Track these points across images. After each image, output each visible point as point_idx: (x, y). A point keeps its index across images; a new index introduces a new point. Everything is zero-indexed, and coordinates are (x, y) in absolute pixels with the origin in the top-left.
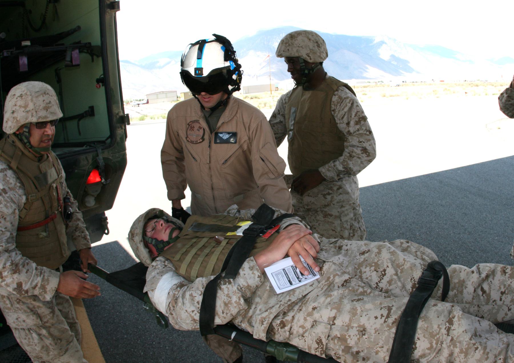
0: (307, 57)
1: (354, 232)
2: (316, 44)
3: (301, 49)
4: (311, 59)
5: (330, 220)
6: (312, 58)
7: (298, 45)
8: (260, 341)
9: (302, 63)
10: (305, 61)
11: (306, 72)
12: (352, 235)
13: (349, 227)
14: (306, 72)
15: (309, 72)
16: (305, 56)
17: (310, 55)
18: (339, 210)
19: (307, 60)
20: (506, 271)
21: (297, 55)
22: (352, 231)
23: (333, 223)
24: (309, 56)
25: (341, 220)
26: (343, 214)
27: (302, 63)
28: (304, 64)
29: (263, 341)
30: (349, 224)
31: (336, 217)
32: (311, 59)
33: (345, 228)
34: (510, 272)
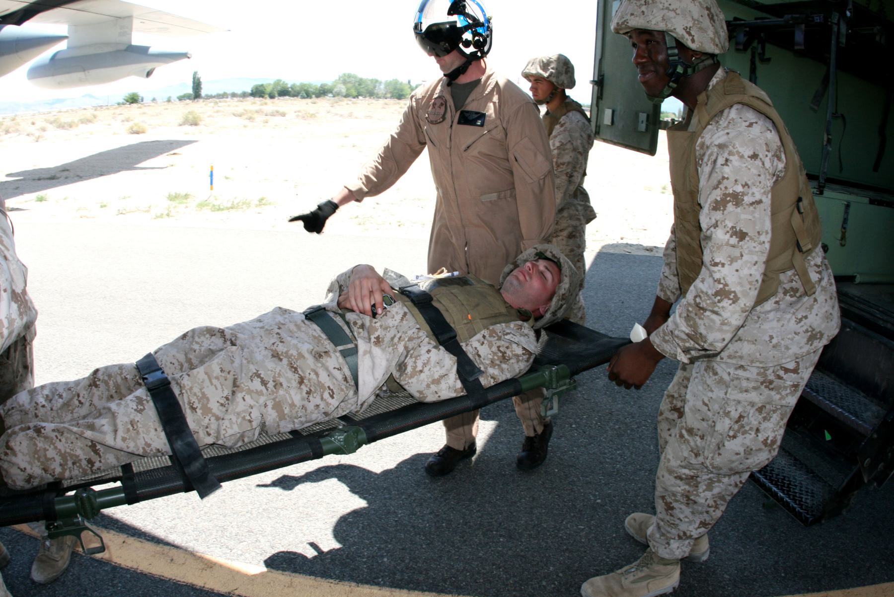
0: (687, 36)
1: (738, 431)
2: (706, 12)
3: (672, 14)
4: (693, 41)
5: (709, 382)
6: (695, 38)
7: (666, 5)
8: (315, 557)
9: (672, 48)
10: (680, 45)
11: (680, 70)
12: (731, 433)
13: (737, 416)
14: (680, 70)
15: (685, 71)
16: (680, 32)
17: (693, 33)
18: (732, 371)
19: (683, 41)
20: (195, 406)
21: (662, 27)
22: (736, 427)
23: (712, 391)
24: (689, 33)
25: (726, 394)
26: (735, 382)
27: (672, 48)
28: (676, 51)
29: (290, 439)
30: (740, 409)
31: (721, 381)
32: (693, 41)
33: (727, 414)
34: (199, 406)
